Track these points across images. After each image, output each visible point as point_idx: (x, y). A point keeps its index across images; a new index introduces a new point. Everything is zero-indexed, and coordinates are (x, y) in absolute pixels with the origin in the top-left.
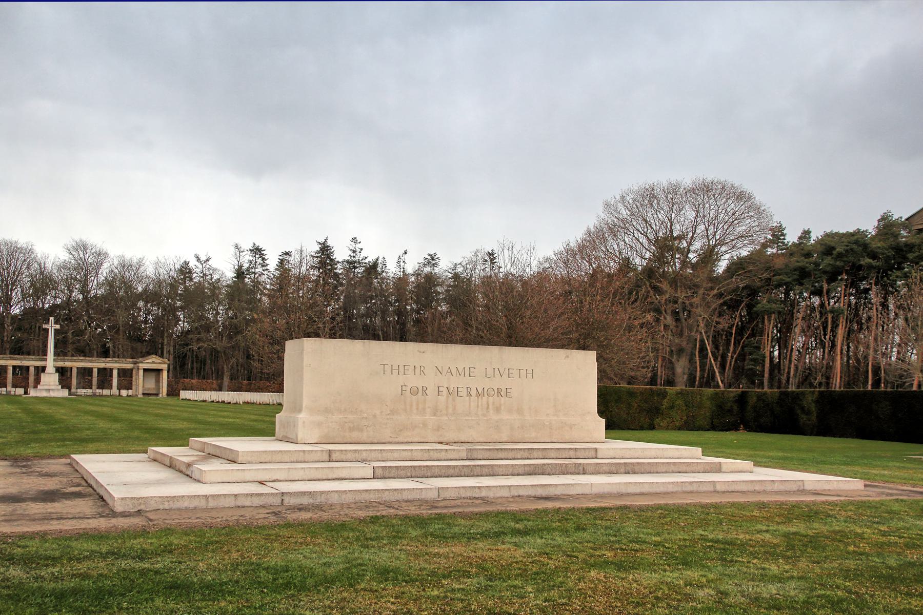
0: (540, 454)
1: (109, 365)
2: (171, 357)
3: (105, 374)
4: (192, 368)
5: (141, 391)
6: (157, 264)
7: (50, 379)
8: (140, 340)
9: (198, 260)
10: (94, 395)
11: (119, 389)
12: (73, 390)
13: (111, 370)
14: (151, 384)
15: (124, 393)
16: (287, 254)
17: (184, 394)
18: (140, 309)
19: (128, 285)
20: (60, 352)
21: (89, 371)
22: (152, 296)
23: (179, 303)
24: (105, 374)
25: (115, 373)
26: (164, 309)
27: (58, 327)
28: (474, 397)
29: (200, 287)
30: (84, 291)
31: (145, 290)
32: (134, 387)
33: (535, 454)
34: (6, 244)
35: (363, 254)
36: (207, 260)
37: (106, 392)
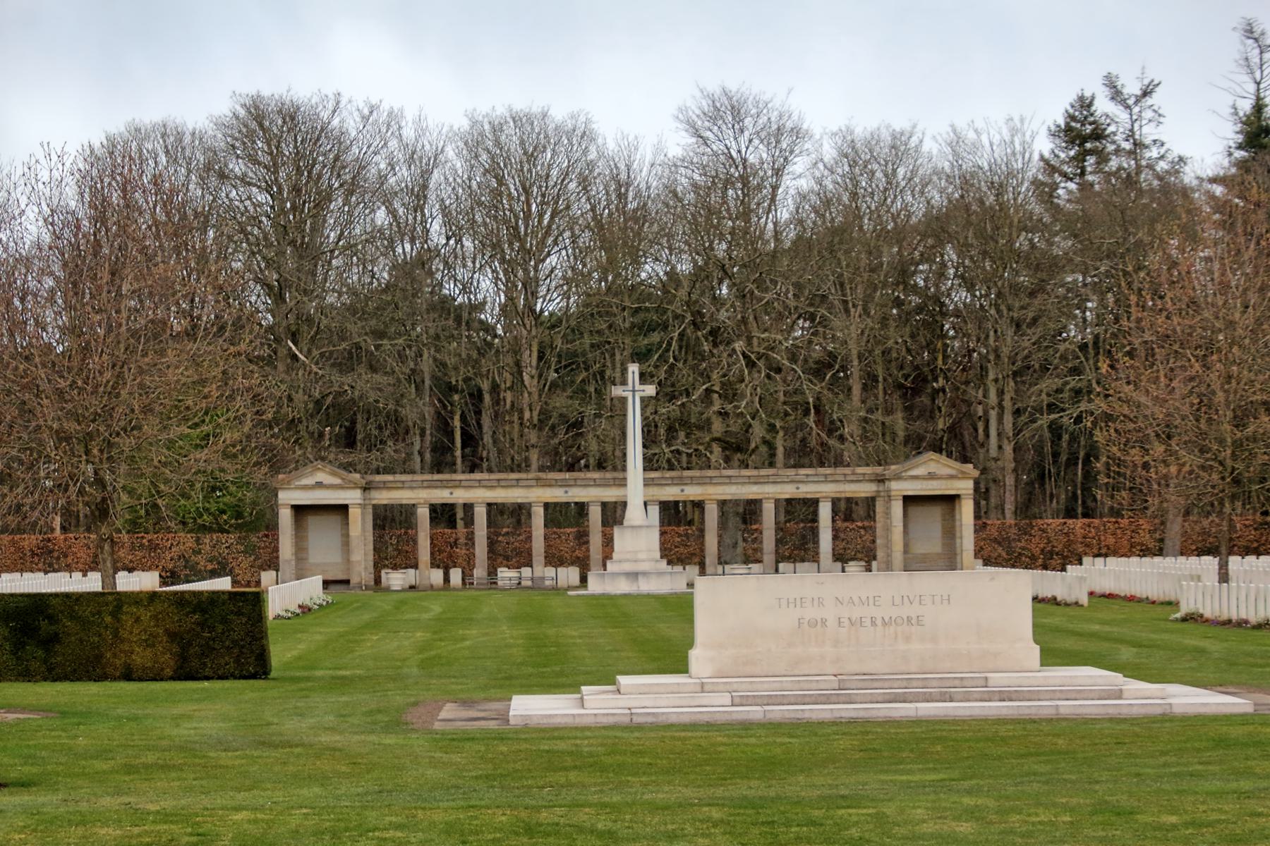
0: (920, 684)
6: (956, 142)
7: (639, 541)
13: (814, 503)
20: (672, 444)
25: (825, 511)
28: (880, 628)
33: (914, 684)
36: (1146, 93)
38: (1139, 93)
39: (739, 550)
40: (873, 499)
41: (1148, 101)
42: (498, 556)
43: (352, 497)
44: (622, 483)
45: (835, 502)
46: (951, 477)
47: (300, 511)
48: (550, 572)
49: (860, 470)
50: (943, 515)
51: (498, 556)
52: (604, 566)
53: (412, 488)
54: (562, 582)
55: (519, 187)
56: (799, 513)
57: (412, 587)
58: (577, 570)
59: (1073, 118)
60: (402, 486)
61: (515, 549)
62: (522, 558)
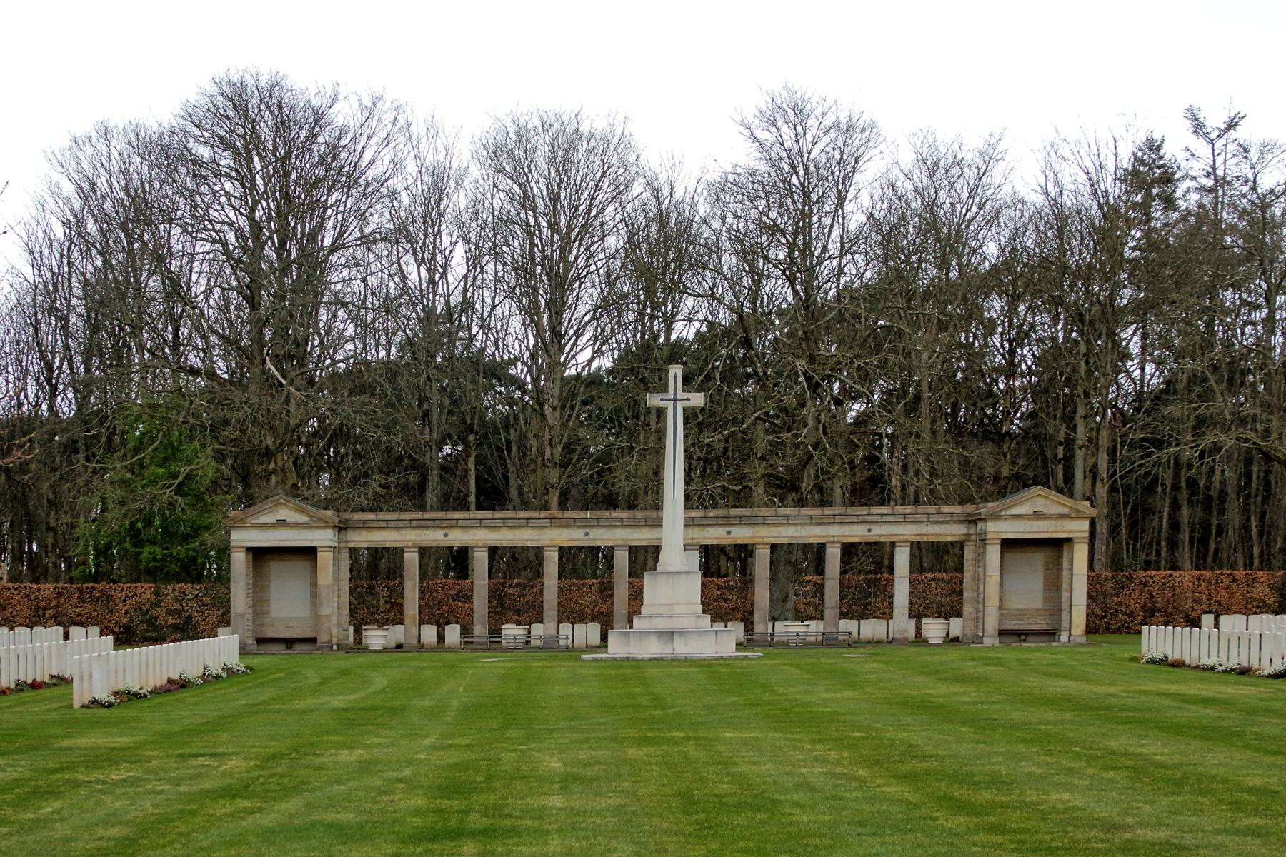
1: (881, 532)
2: (1102, 491)
4: (1175, 526)
5: (992, 624)
7: (675, 591)
8: (992, 433)
9: (1198, 127)
10: (830, 642)
11: (916, 615)
12: (759, 628)
13: (609, 553)
14: (1027, 593)
15: (934, 630)
17: (1157, 641)
18: (990, 327)
19: (947, 238)
20: (721, 476)
21: (459, 560)
22: (1028, 278)
23: (1125, 296)
24: (868, 562)
25: (902, 559)
26: (1078, 318)
27: (697, 399)
29: (1205, 224)
30: (801, 268)
31: (1011, 255)
32: (967, 609)
34: (546, 126)
36: (1231, 126)
37: (871, 628)
38: (1223, 126)
39: (790, 605)
40: (962, 545)
41: (1233, 134)
42: (502, 609)
43: (322, 538)
44: (657, 523)
45: (918, 549)
46: (1063, 517)
47: (259, 555)
48: (566, 629)
49: (947, 509)
50: (1046, 564)
51: (502, 609)
52: (631, 622)
53: (397, 528)
54: (580, 641)
55: (553, 206)
57: (399, 647)
58: (598, 626)
59: (1142, 162)
60: (386, 526)
61: (528, 602)
62: (530, 613)
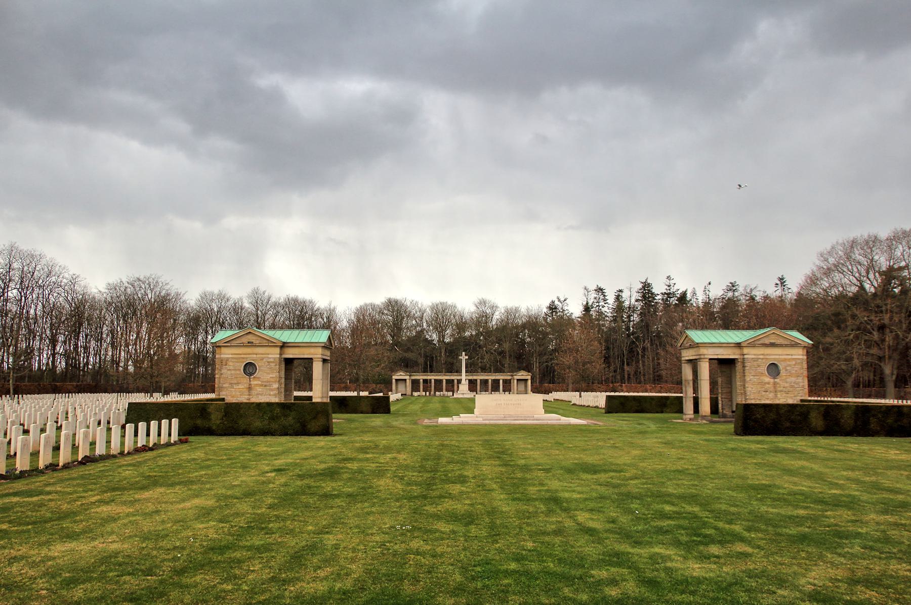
3: (507, 383)
7: (464, 387)
9: (559, 300)
13: (499, 380)
16: (621, 291)
25: (501, 382)
35: (676, 287)
56: (496, 382)
